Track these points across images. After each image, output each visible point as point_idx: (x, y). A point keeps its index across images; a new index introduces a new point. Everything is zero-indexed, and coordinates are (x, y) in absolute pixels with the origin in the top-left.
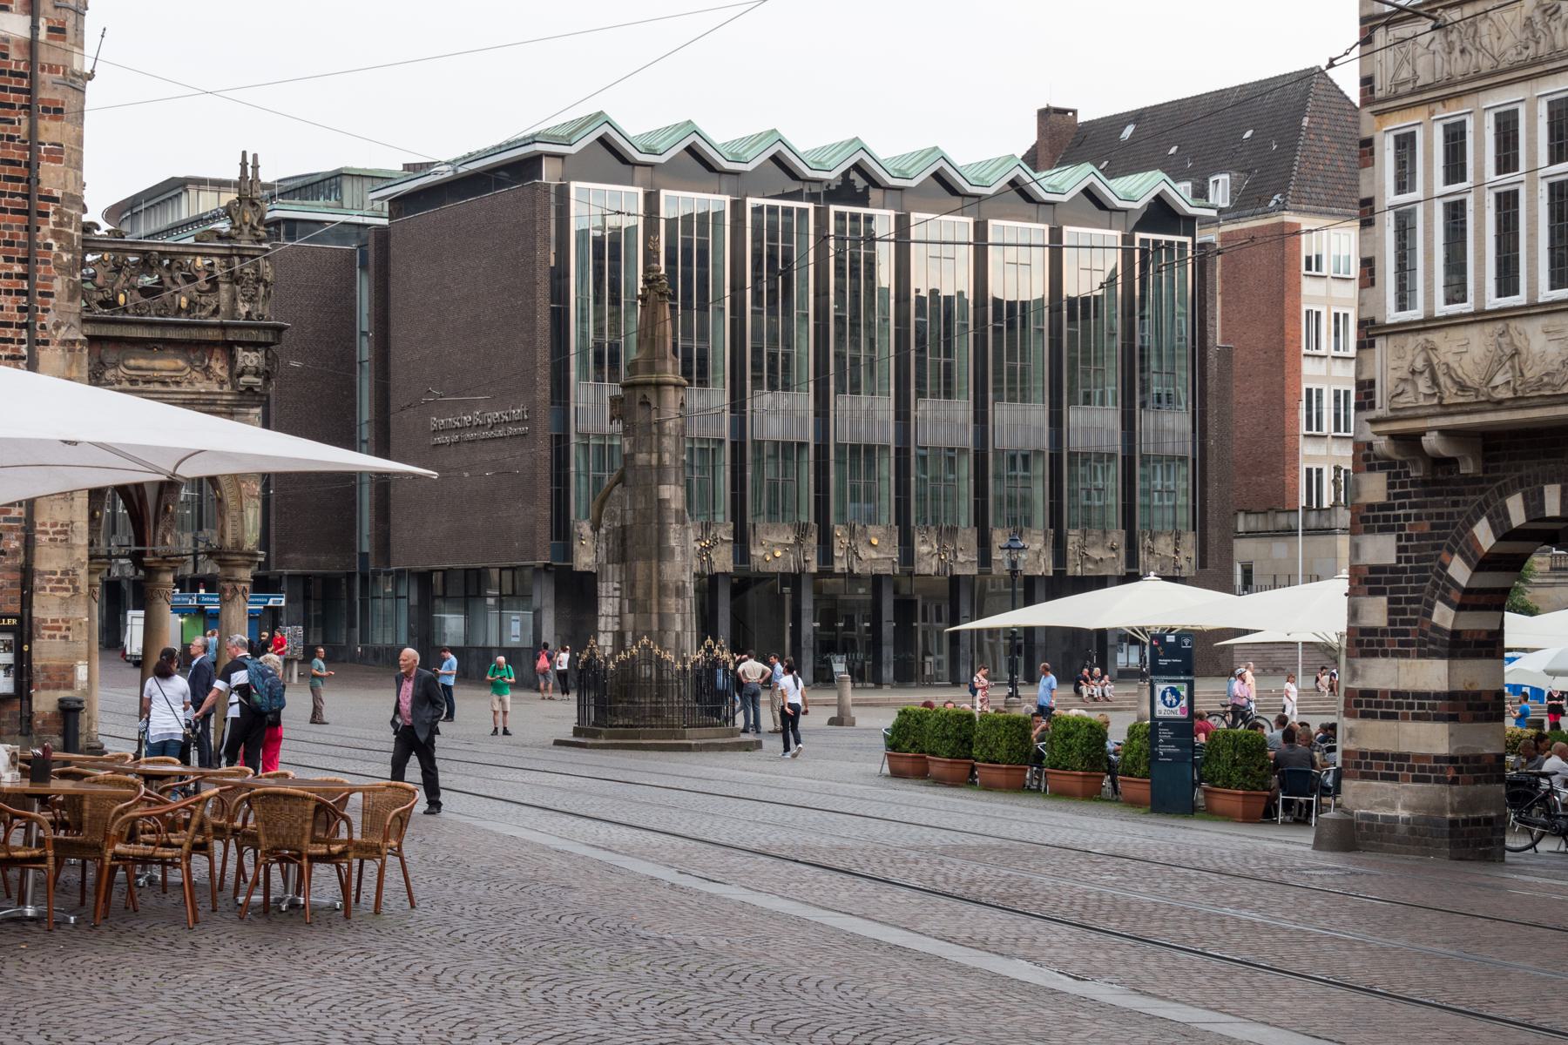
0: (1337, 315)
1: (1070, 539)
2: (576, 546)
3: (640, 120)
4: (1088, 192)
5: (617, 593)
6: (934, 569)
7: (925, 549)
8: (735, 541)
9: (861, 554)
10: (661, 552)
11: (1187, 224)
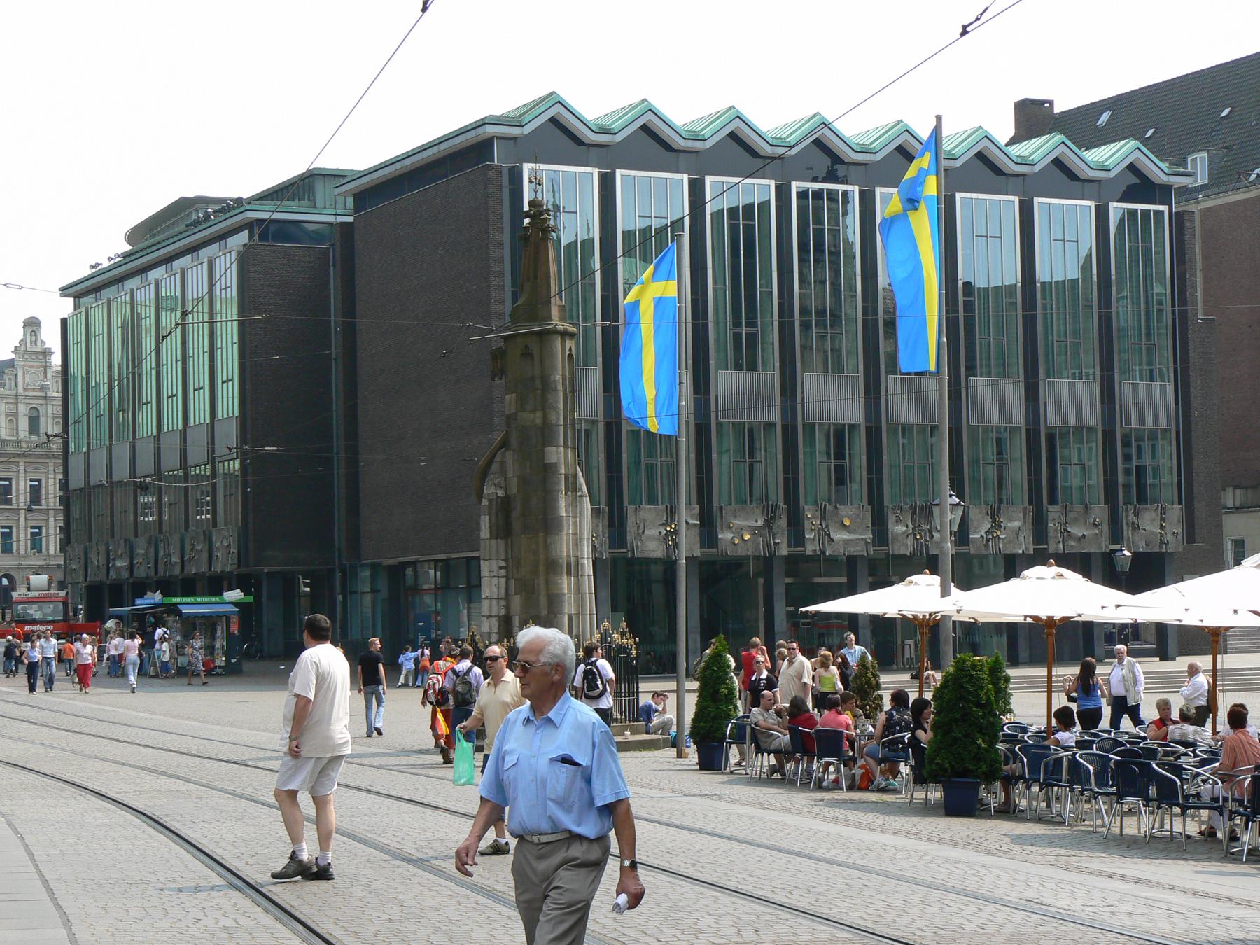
1: (1051, 516)
3: (597, 102)
4: (1057, 162)
5: (503, 572)
7: (900, 529)
8: (702, 525)
9: (833, 535)
10: (548, 524)
11: (1160, 193)
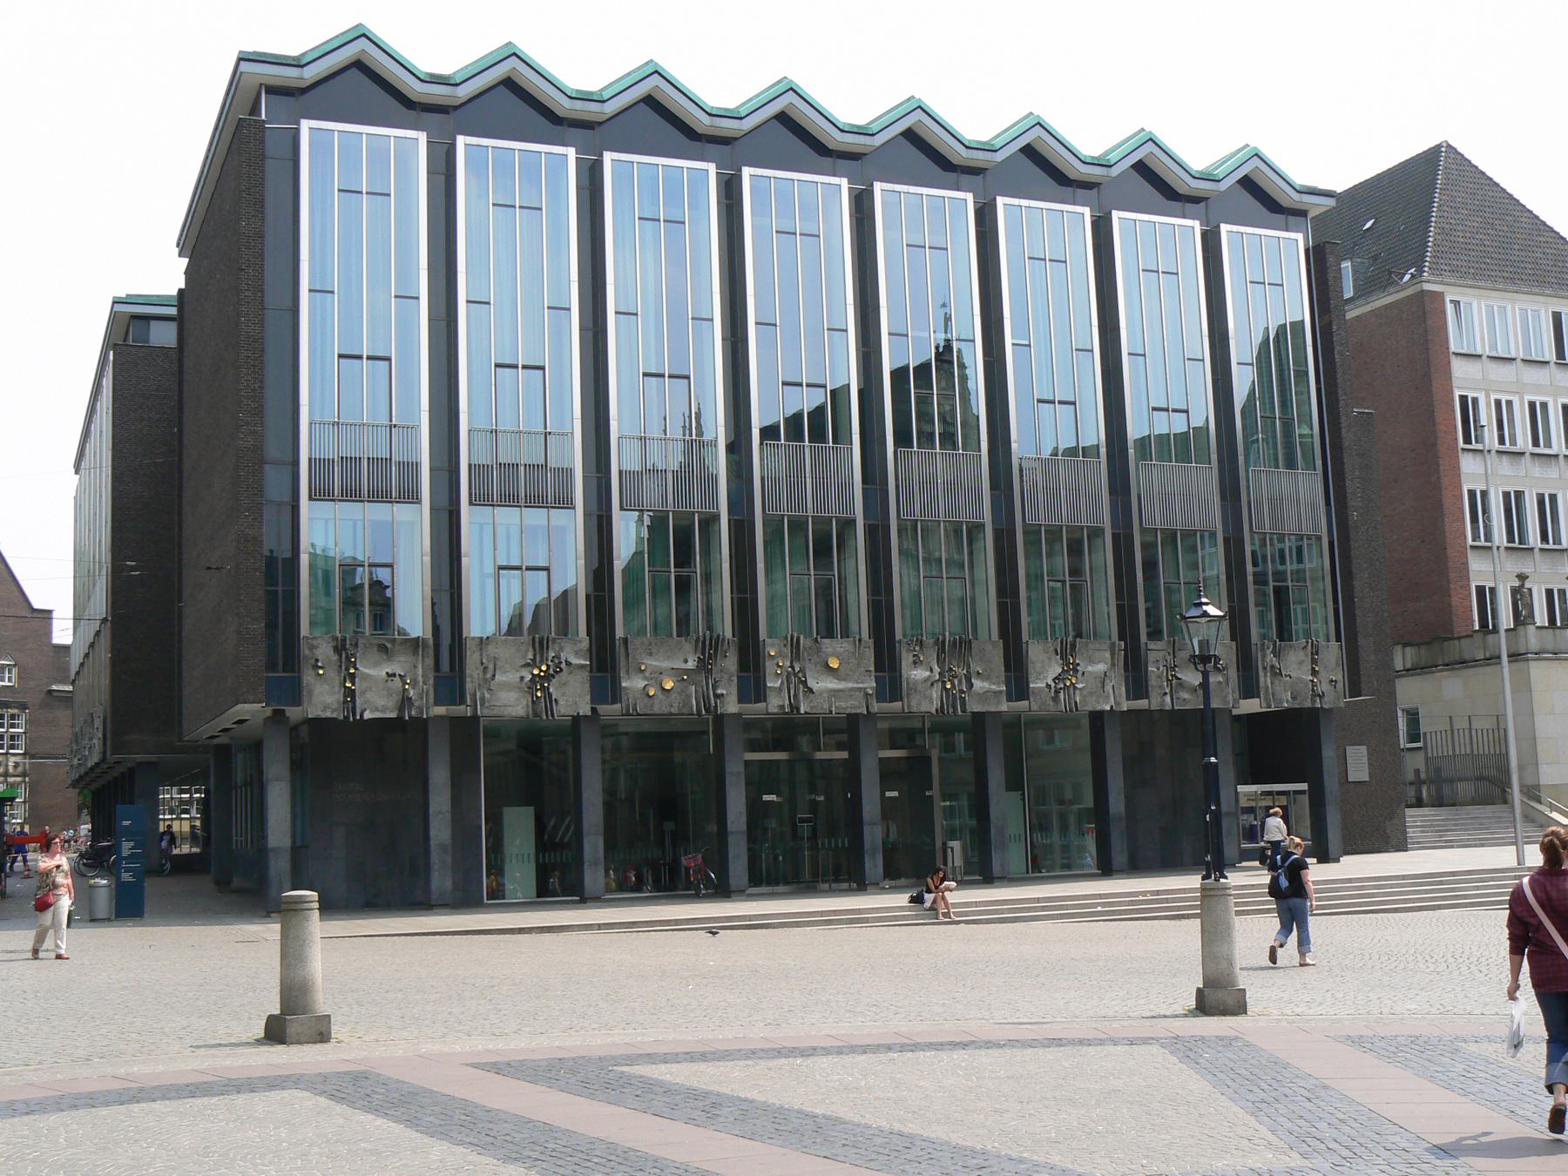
0: (1498, 403)
1: (1152, 657)
2: (308, 677)
6: (936, 704)
7: (920, 674)
9: (811, 683)
